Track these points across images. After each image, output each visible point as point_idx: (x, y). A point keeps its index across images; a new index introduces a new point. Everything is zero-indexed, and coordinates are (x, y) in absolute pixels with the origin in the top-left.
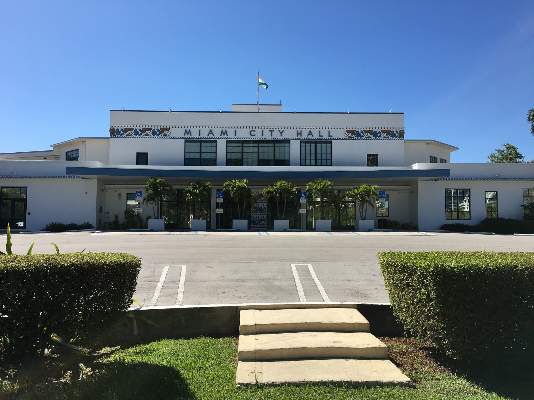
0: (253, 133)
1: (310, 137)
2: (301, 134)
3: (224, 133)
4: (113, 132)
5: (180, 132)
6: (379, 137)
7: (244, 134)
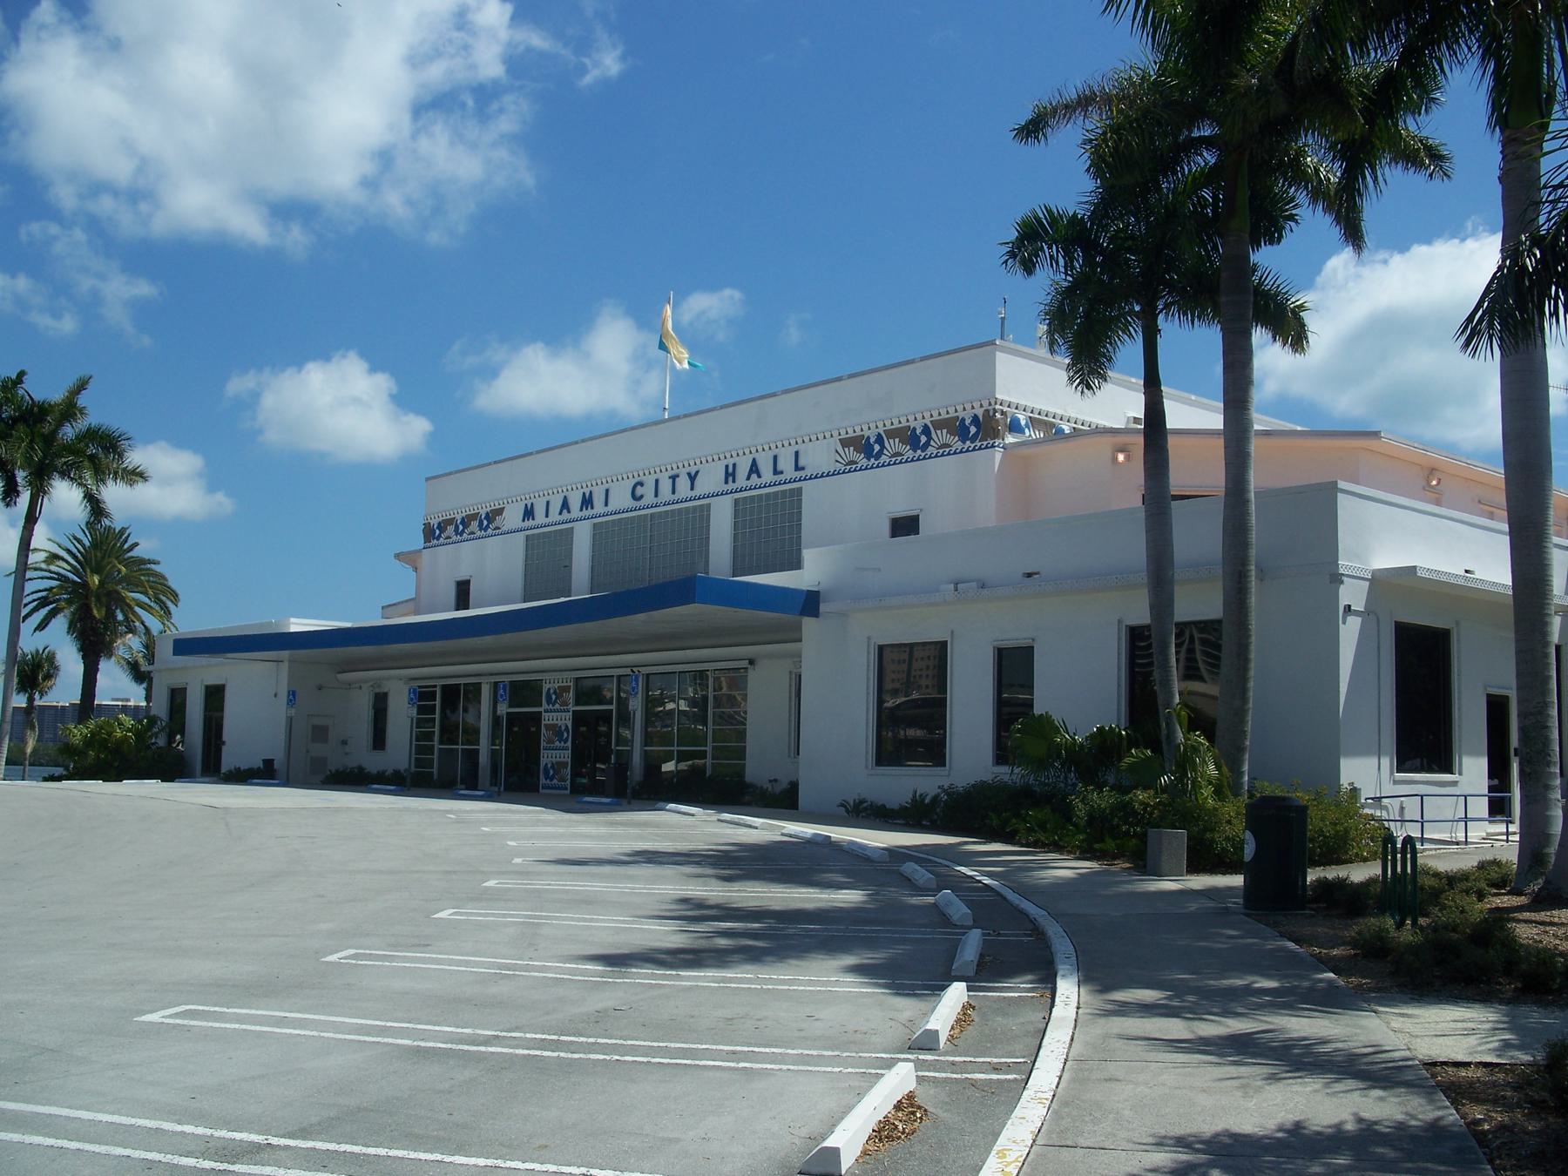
0: (639, 490)
1: (754, 479)
2: (733, 475)
3: (587, 502)
4: (430, 533)
5: (512, 517)
6: (878, 456)
7: (621, 499)
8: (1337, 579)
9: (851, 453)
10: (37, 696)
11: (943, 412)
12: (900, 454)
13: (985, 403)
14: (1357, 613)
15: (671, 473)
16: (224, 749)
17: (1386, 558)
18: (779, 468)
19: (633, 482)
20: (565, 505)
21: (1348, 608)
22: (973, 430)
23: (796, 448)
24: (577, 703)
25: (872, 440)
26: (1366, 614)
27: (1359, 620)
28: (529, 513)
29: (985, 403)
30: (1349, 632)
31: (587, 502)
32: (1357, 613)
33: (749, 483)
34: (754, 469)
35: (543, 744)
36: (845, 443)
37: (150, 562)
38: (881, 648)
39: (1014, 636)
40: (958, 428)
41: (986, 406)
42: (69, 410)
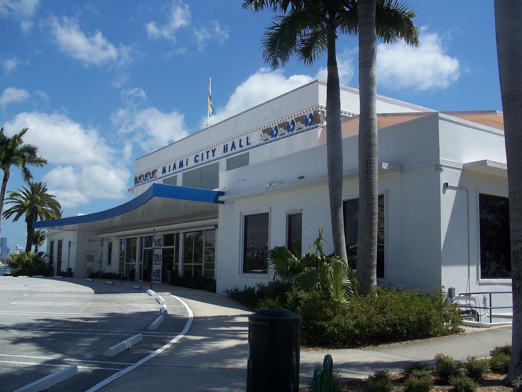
0: (197, 158)
2: (227, 149)
3: (181, 165)
6: (275, 136)
8: (438, 168)
9: (266, 136)
10: (38, 246)
11: (299, 114)
12: (283, 134)
13: (315, 108)
14: (452, 188)
15: (207, 150)
16: (62, 264)
17: (470, 158)
18: (242, 145)
19: (195, 155)
20: (175, 167)
21: (446, 185)
22: (310, 120)
23: (247, 135)
24: (165, 245)
25: (273, 129)
26: (460, 188)
27: (455, 192)
28: (164, 171)
29: (315, 108)
30: (447, 201)
31: (181, 165)
32: (452, 188)
33: (231, 152)
34: (233, 146)
35: (154, 262)
36: (264, 131)
37: (53, 196)
38: (246, 217)
39: (294, 209)
40: (304, 120)
41: (315, 109)
42: (17, 138)
